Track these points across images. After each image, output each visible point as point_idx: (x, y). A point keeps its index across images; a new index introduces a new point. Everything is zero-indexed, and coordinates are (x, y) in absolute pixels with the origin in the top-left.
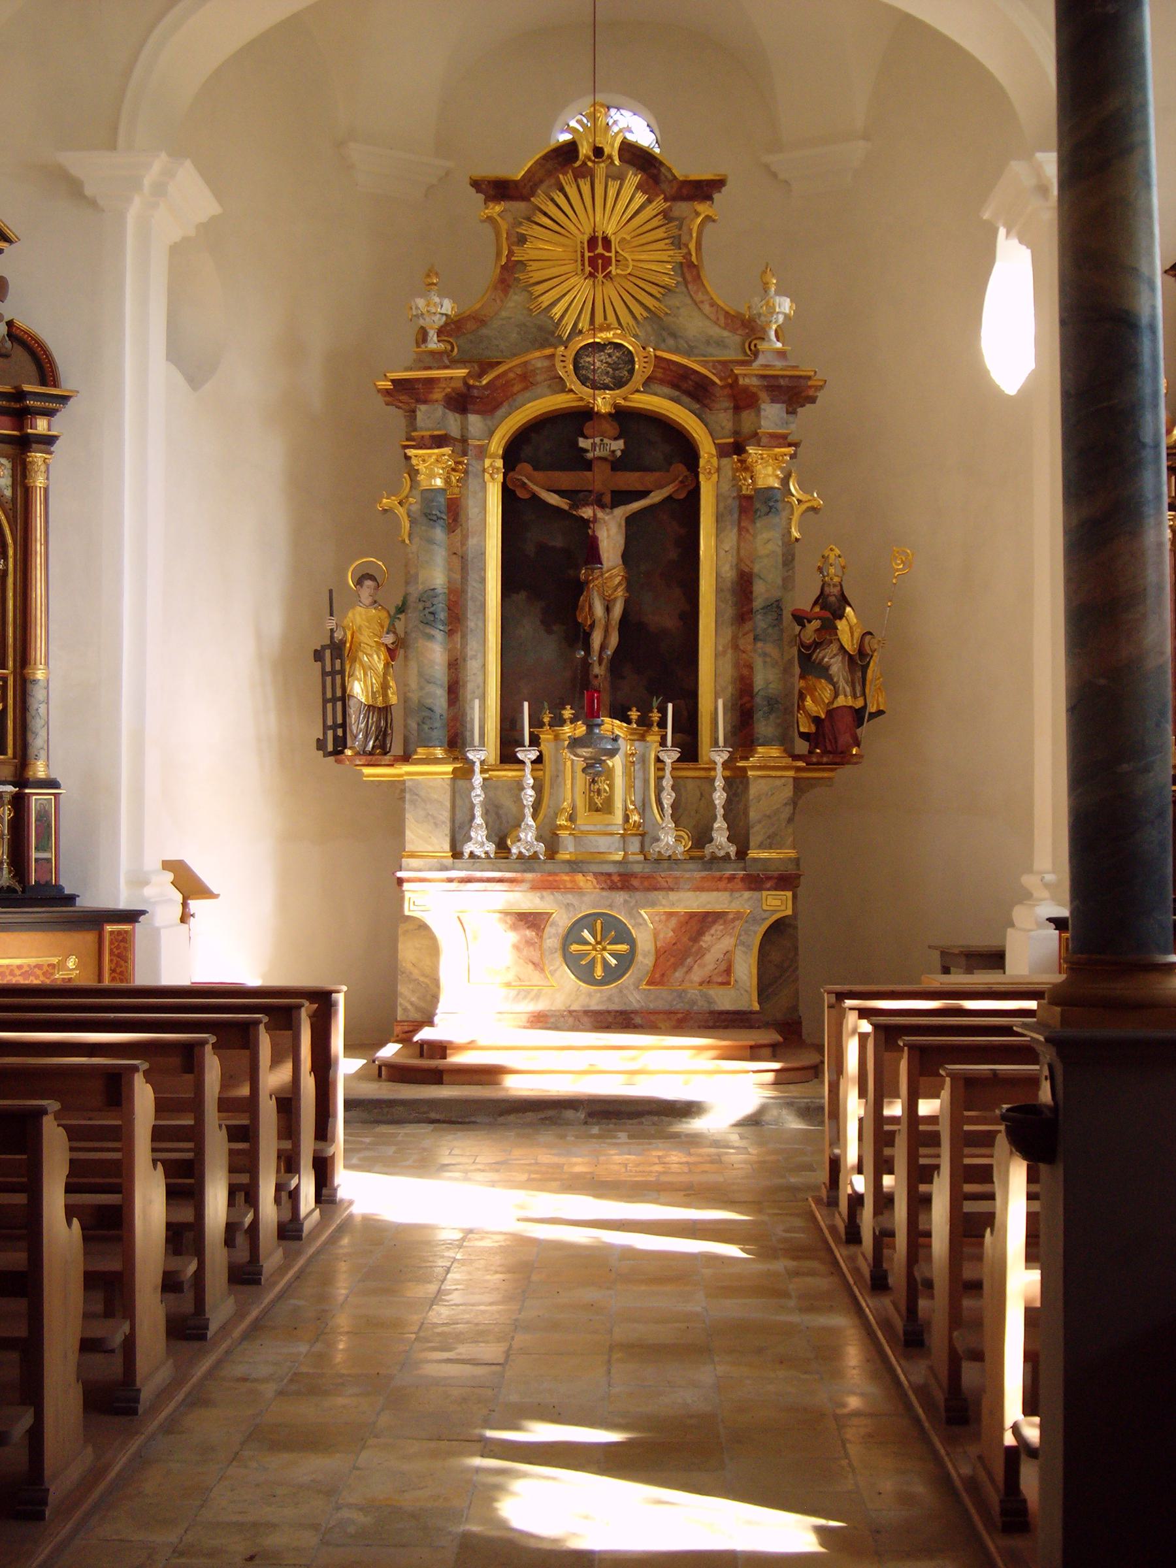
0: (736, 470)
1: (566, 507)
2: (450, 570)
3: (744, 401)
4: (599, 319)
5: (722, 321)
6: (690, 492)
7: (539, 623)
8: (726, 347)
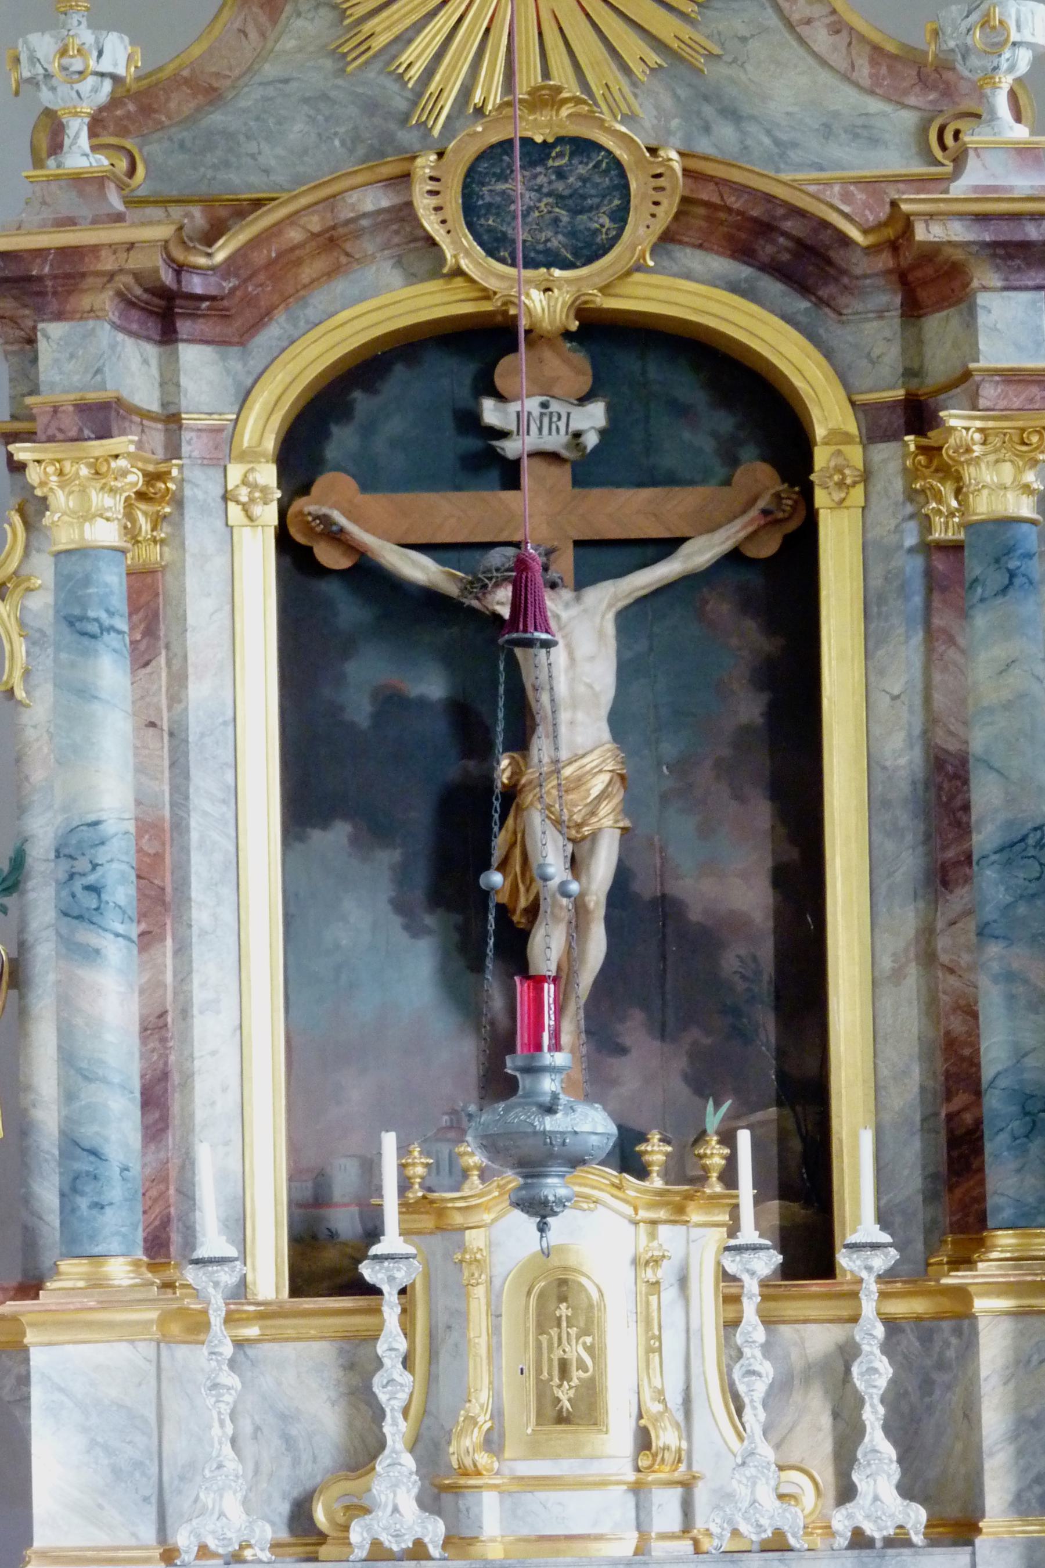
0: (910, 474)
1: (452, 590)
2: (140, 769)
3: (928, 284)
4: (528, 77)
5: (864, 71)
6: (788, 540)
7: (383, 906)
8: (874, 142)
